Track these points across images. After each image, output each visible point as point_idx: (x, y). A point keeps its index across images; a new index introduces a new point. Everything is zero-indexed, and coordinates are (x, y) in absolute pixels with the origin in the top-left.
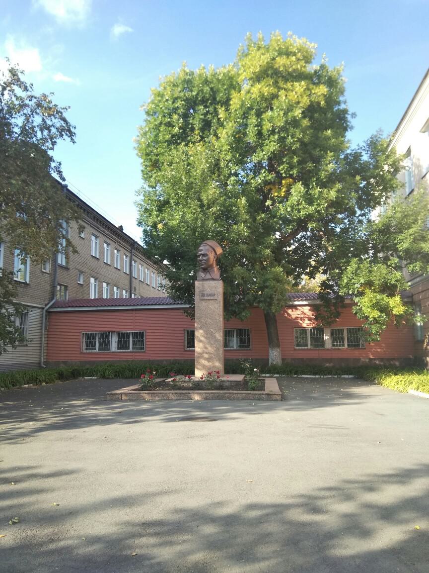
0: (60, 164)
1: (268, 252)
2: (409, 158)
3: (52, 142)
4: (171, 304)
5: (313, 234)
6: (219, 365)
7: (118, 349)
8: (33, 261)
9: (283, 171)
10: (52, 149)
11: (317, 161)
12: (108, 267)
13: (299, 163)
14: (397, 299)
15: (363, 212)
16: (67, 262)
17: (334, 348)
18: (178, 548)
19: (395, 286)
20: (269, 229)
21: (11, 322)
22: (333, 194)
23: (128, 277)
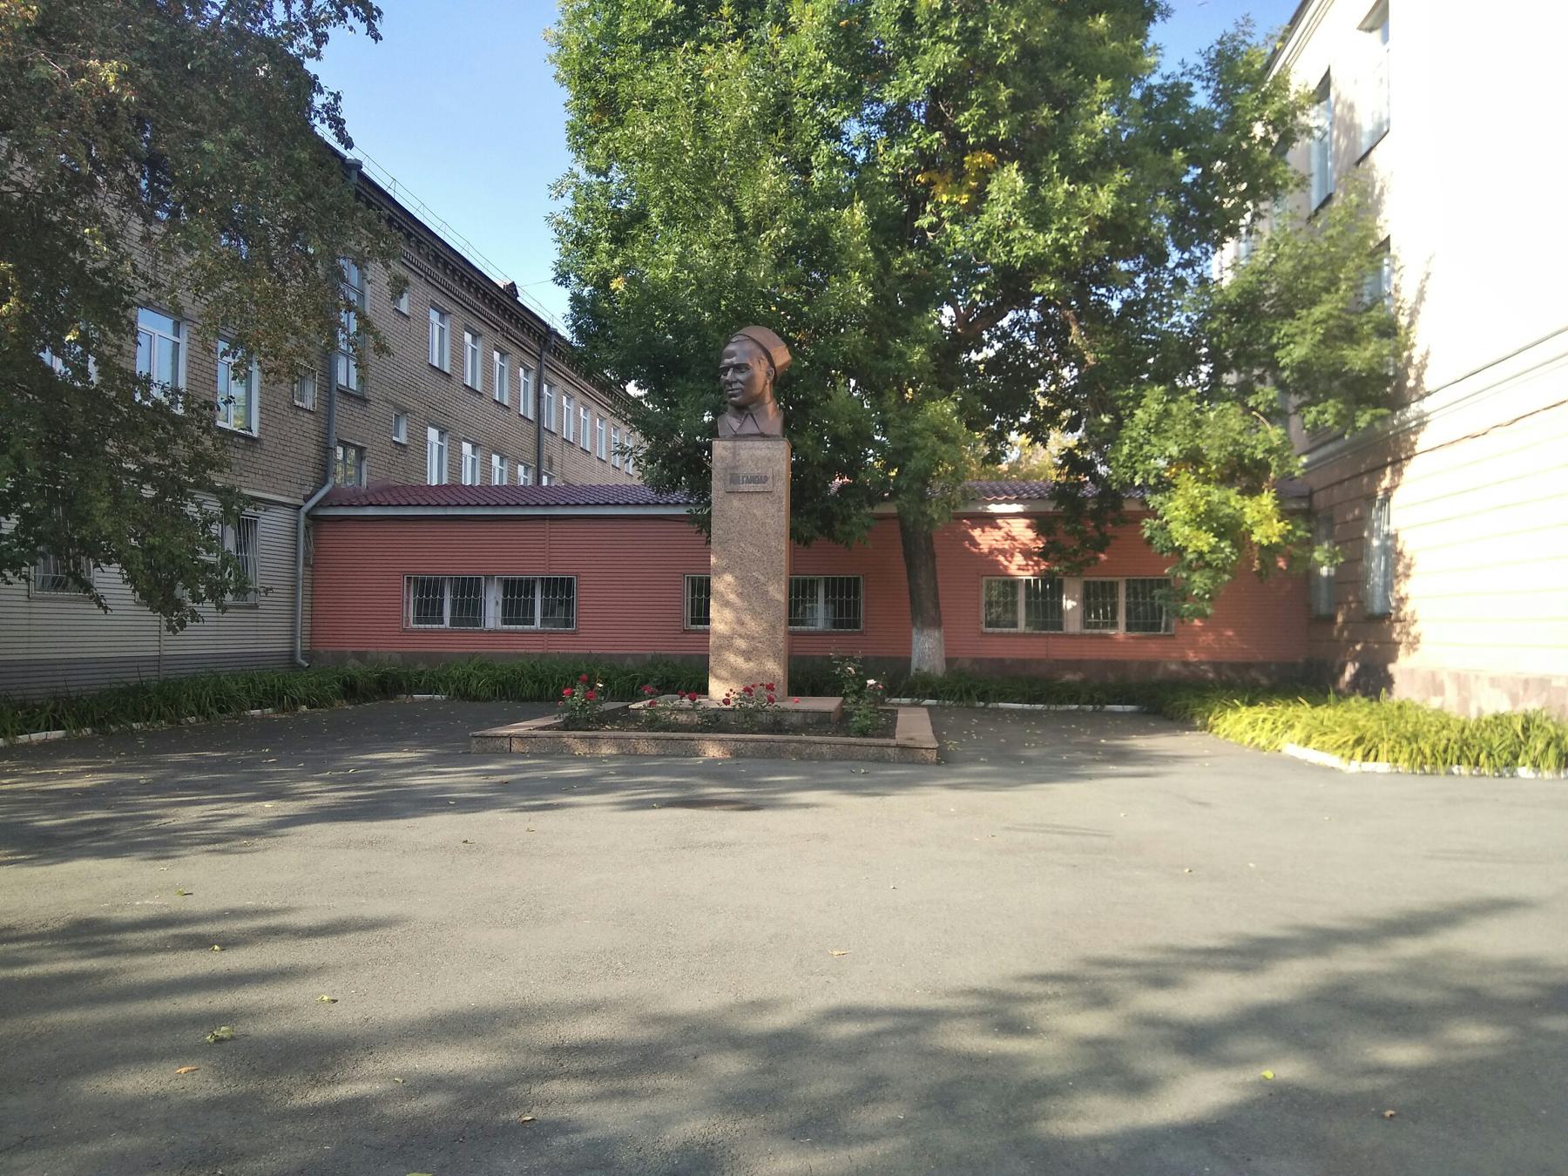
0: (337, 97)
1: (917, 355)
2: (1324, 103)
3: (315, 34)
4: (648, 504)
5: (1045, 315)
6: (774, 668)
7: (505, 622)
8: (265, 372)
9: (969, 128)
10: (316, 55)
11: (1065, 103)
12: (476, 398)
13: (1016, 104)
14: (1267, 500)
15: (1186, 256)
16: (361, 379)
17: (1088, 631)
18: (643, 1107)
19: (1263, 466)
20: (925, 295)
21: (210, 538)
22: (1105, 200)
23: (532, 429)
